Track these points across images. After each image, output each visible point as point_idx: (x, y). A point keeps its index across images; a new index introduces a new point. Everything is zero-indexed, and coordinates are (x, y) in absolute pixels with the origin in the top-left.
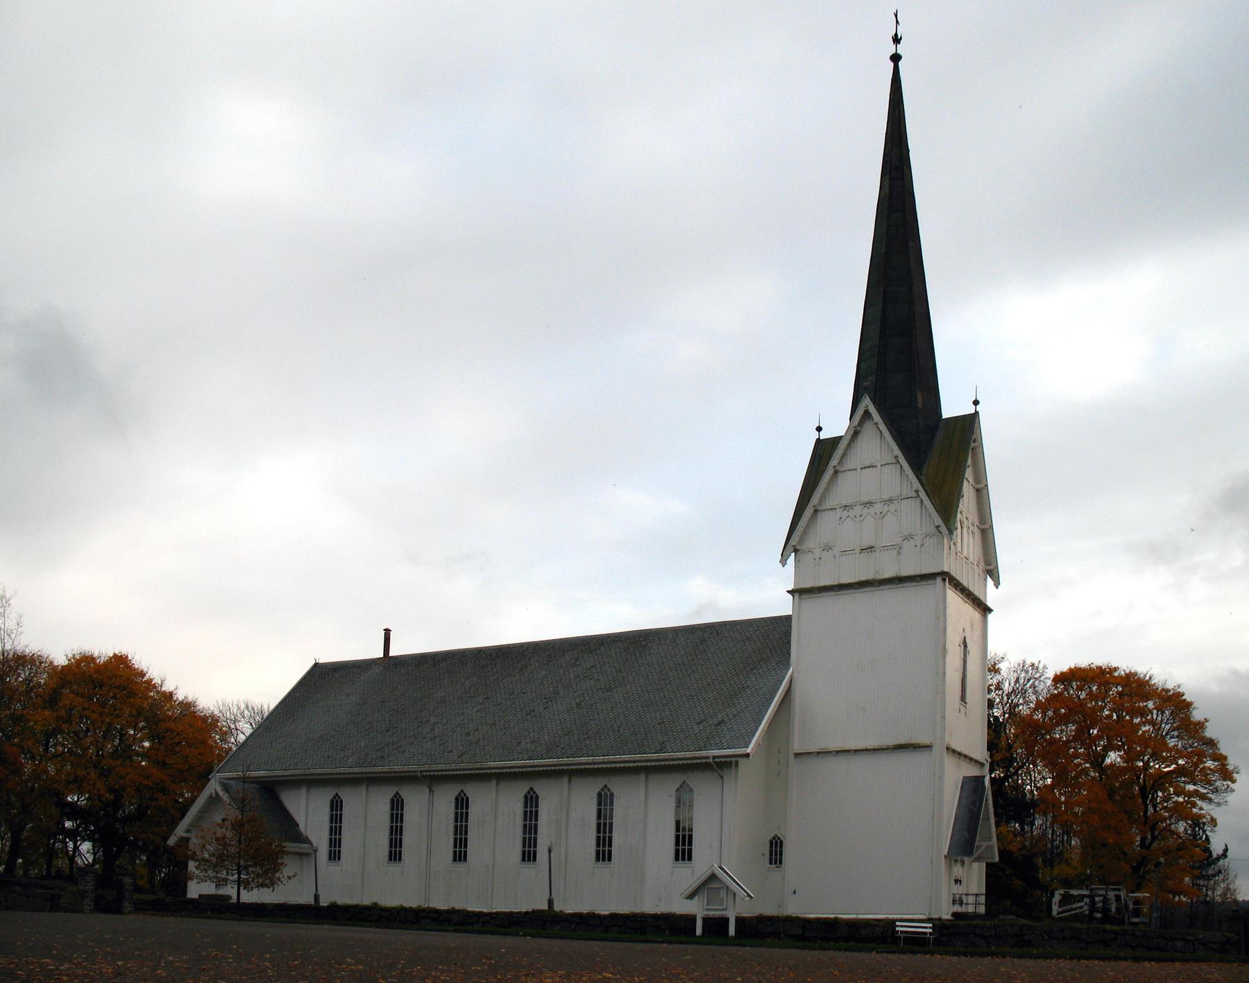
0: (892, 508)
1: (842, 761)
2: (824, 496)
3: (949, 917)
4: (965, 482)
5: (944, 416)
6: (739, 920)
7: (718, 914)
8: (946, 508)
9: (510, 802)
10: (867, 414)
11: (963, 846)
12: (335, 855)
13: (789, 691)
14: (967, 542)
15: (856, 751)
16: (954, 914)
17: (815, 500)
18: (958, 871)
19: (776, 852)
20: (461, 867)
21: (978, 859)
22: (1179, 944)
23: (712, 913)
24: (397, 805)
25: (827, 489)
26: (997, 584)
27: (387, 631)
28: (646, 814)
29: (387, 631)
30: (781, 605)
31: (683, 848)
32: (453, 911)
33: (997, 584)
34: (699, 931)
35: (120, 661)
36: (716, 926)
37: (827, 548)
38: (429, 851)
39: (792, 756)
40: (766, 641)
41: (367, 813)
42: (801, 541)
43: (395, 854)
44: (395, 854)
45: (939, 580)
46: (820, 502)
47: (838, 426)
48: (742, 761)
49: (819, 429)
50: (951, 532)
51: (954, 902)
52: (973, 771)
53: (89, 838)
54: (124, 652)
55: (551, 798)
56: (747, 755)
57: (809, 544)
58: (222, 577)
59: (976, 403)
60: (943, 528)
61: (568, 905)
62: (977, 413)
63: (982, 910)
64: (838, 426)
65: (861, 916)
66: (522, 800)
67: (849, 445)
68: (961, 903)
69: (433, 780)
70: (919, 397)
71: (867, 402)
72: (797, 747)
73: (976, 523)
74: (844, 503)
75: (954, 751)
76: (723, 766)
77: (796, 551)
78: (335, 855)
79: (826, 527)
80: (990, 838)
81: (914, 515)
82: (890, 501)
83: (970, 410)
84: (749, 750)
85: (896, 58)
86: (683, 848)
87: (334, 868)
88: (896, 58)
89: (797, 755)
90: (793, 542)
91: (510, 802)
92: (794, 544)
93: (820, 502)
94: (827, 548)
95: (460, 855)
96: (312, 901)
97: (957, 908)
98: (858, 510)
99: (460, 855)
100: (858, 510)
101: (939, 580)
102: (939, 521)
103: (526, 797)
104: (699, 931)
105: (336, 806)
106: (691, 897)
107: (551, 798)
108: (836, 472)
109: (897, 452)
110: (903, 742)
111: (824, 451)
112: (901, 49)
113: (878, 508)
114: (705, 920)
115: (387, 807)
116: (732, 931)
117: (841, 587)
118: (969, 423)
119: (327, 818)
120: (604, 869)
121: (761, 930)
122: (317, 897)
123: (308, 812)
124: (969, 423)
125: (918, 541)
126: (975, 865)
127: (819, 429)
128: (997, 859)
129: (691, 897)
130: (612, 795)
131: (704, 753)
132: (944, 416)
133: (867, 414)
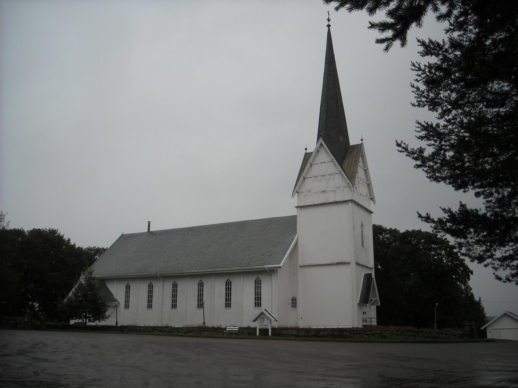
0: (332, 177)
1: (317, 269)
2: (307, 173)
3: (361, 327)
4: (359, 167)
5: (351, 144)
6: (273, 329)
7: (265, 327)
8: (351, 176)
9: (168, 287)
10: (321, 144)
11: (365, 300)
12: (127, 306)
13: (296, 244)
14: (363, 189)
15: (316, 265)
16: (363, 326)
17: (304, 174)
18: (364, 309)
19: (294, 302)
20: (174, 310)
21: (372, 305)
22: (444, 336)
23: (262, 327)
24: (151, 287)
25: (308, 170)
26: (375, 203)
27: (149, 222)
28: (244, 290)
29: (149, 222)
30: (292, 212)
31: (258, 302)
32: (166, 327)
33: (375, 203)
34: (258, 334)
35: (53, 232)
36: (264, 332)
37: (309, 191)
38: (162, 304)
39: (298, 267)
40: (289, 224)
41: (139, 291)
42: (299, 189)
43: (150, 306)
44: (150, 306)
45: (350, 203)
46: (306, 175)
47: (312, 147)
48: (279, 269)
49: (306, 149)
50: (353, 185)
51: (363, 321)
52: (368, 272)
53: (38, 302)
54: (55, 228)
55: (208, 284)
56: (280, 267)
57: (302, 190)
58: (92, 201)
59: (362, 140)
60: (350, 184)
61: (209, 324)
62: (362, 143)
63: (374, 323)
64: (312, 147)
65: (319, 327)
66: (254, 282)
67: (315, 156)
68: (366, 321)
69: (165, 277)
70: (341, 138)
71: (321, 140)
72: (301, 263)
73: (365, 181)
74: (314, 175)
75: (359, 264)
76: (271, 272)
77: (297, 192)
78: (127, 306)
79: (309, 184)
80: (376, 296)
81: (339, 180)
82: (331, 174)
83: (360, 142)
84: (281, 265)
85: (329, 26)
86: (258, 302)
87: (126, 311)
88: (329, 26)
89: (301, 267)
90: (296, 189)
91: (168, 287)
92: (296, 191)
93: (306, 175)
94: (309, 191)
95: (174, 306)
96: (114, 324)
97: (365, 323)
98: (327, 177)
99: (174, 306)
100: (319, 178)
101: (350, 203)
102: (349, 182)
103: (226, 282)
104: (258, 334)
105: (128, 288)
106: (255, 321)
107: (208, 284)
108: (311, 165)
109: (333, 157)
110: (339, 261)
111: (307, 156)
112: (330, 23)
113: (327, 177)
114: (260, 329)
115: (147, 288)
116: (270, 334)
117: (315, 205)
118: (359, 148)
119: (124, 292)
120: (228, 310)
121: (280, 333)
122: (117, 323)
123: (117, 291)
124: (359, 148)
125: (342, 188)
126: (372, 307)
127: (306, 149)
128: (379, 304)
129: (255, 321)
130: (260, 281)
131: (265, 267)
132: (351, 144)
133: (321, 144)
